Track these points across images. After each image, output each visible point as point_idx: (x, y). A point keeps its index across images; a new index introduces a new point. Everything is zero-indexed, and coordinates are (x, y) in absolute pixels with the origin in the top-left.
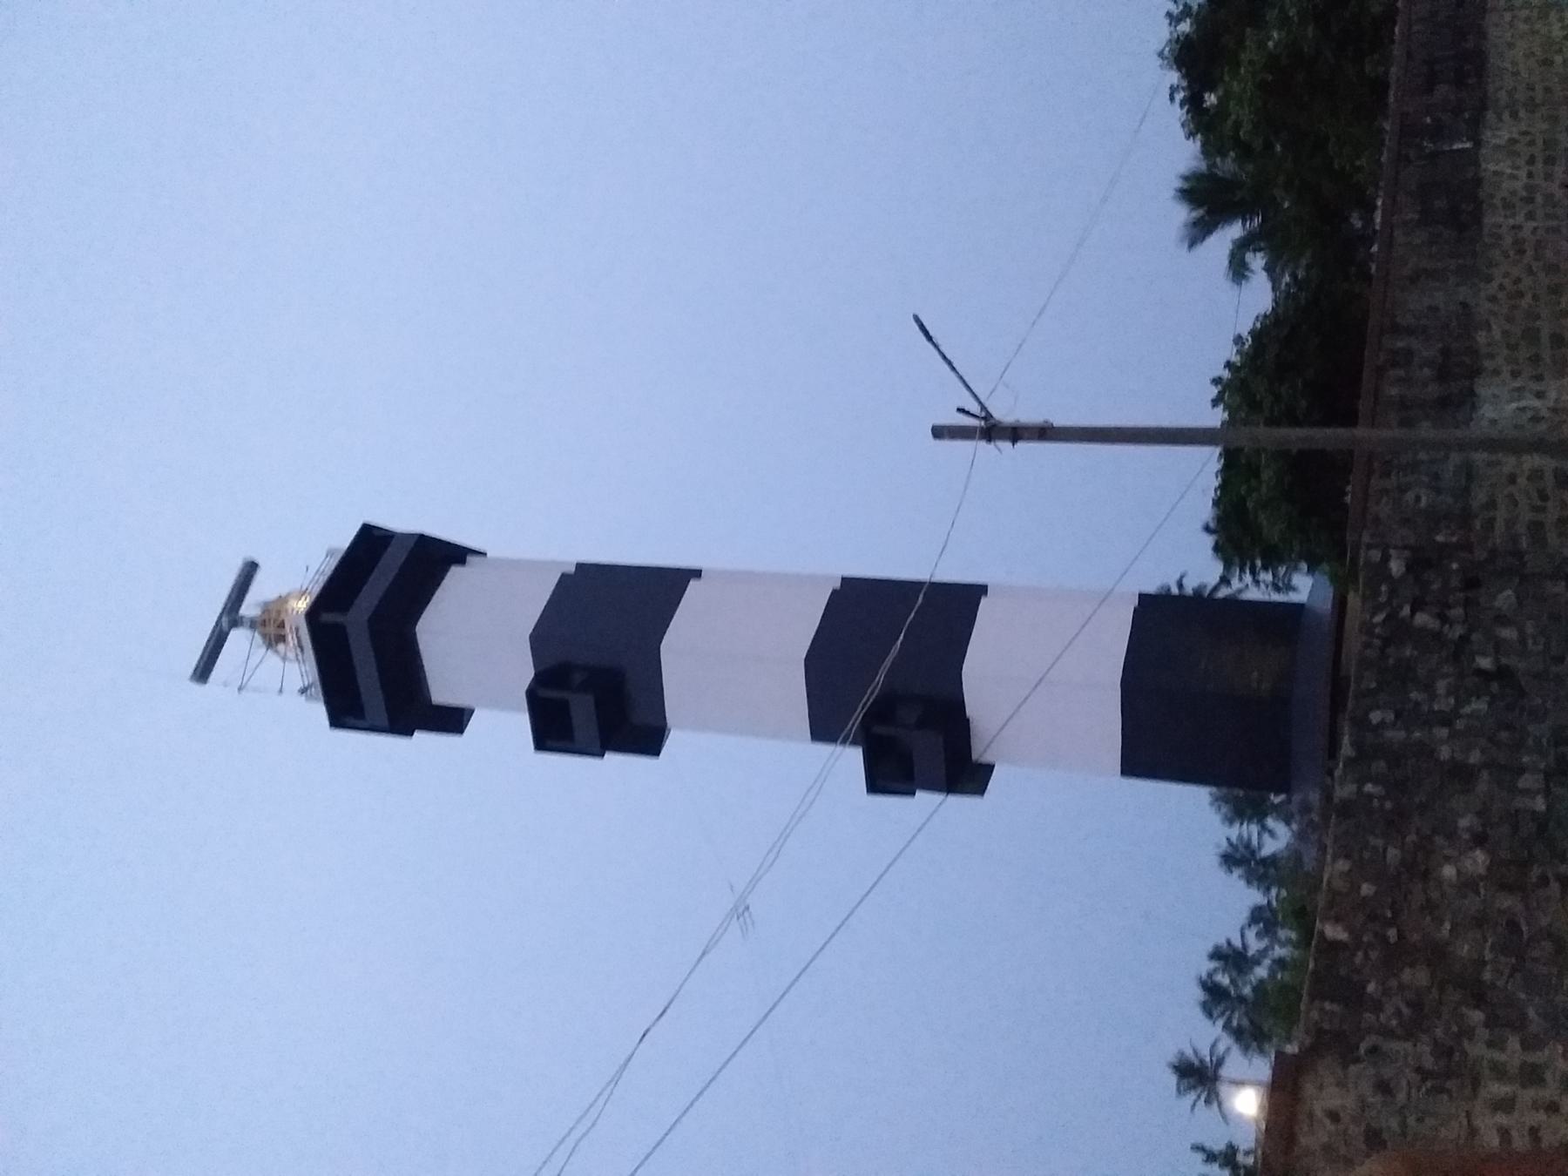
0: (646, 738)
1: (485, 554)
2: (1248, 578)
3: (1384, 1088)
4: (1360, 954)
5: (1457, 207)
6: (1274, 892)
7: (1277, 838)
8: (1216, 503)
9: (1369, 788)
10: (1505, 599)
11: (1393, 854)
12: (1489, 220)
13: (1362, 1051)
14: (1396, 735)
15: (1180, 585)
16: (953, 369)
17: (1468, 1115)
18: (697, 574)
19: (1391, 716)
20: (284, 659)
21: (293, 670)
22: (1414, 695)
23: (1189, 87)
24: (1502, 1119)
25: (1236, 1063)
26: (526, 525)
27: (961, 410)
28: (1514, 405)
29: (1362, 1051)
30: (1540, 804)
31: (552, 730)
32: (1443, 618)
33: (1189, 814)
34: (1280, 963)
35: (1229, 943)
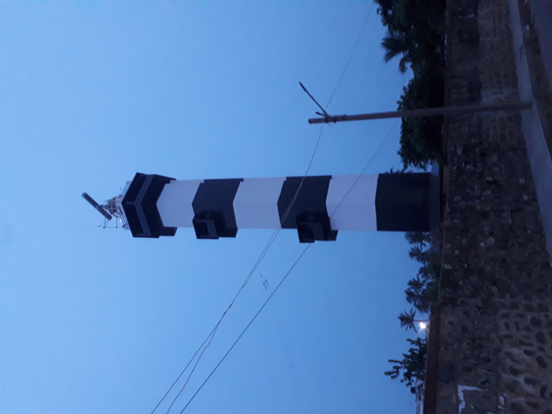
0: (231, 232)
1: (175, 179)
2: (412, 165)
3: (466, 313)
4: (456, 273)
5: (471, 38)
6: (426, 263)
7: (426, 247)
8: (401, 142)
9: (455, 221)
10: (494, 158)
11: (464, 241)
12: (481, 39)
13: (459, 302)
14: (463, 204)
15: (391, 171)
16: (313, 99)
17: (495, 320)
18: (242, 180)
19: (460, 198)
20: (117, 217)
21: (120, 220)
22: (467, 191)
23: (383, 8)
24: (506, 320)
25: (418, 315)
26: (187, 168)
27: (318, 113)
28: (493, 97)
29: (459, 302)
30: (510, 221)
31: (202, 232)
32: (475, 166)
33: (398, 241)
34: (430, 284)
35: (414, 279)
